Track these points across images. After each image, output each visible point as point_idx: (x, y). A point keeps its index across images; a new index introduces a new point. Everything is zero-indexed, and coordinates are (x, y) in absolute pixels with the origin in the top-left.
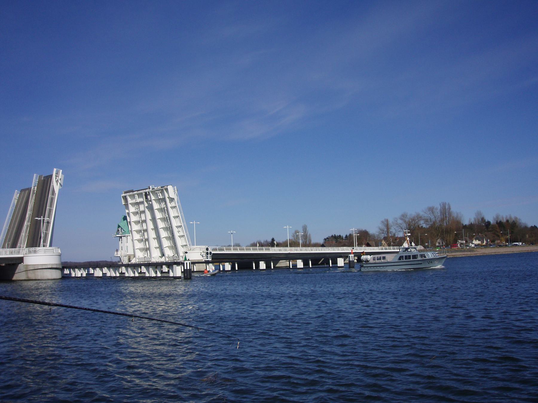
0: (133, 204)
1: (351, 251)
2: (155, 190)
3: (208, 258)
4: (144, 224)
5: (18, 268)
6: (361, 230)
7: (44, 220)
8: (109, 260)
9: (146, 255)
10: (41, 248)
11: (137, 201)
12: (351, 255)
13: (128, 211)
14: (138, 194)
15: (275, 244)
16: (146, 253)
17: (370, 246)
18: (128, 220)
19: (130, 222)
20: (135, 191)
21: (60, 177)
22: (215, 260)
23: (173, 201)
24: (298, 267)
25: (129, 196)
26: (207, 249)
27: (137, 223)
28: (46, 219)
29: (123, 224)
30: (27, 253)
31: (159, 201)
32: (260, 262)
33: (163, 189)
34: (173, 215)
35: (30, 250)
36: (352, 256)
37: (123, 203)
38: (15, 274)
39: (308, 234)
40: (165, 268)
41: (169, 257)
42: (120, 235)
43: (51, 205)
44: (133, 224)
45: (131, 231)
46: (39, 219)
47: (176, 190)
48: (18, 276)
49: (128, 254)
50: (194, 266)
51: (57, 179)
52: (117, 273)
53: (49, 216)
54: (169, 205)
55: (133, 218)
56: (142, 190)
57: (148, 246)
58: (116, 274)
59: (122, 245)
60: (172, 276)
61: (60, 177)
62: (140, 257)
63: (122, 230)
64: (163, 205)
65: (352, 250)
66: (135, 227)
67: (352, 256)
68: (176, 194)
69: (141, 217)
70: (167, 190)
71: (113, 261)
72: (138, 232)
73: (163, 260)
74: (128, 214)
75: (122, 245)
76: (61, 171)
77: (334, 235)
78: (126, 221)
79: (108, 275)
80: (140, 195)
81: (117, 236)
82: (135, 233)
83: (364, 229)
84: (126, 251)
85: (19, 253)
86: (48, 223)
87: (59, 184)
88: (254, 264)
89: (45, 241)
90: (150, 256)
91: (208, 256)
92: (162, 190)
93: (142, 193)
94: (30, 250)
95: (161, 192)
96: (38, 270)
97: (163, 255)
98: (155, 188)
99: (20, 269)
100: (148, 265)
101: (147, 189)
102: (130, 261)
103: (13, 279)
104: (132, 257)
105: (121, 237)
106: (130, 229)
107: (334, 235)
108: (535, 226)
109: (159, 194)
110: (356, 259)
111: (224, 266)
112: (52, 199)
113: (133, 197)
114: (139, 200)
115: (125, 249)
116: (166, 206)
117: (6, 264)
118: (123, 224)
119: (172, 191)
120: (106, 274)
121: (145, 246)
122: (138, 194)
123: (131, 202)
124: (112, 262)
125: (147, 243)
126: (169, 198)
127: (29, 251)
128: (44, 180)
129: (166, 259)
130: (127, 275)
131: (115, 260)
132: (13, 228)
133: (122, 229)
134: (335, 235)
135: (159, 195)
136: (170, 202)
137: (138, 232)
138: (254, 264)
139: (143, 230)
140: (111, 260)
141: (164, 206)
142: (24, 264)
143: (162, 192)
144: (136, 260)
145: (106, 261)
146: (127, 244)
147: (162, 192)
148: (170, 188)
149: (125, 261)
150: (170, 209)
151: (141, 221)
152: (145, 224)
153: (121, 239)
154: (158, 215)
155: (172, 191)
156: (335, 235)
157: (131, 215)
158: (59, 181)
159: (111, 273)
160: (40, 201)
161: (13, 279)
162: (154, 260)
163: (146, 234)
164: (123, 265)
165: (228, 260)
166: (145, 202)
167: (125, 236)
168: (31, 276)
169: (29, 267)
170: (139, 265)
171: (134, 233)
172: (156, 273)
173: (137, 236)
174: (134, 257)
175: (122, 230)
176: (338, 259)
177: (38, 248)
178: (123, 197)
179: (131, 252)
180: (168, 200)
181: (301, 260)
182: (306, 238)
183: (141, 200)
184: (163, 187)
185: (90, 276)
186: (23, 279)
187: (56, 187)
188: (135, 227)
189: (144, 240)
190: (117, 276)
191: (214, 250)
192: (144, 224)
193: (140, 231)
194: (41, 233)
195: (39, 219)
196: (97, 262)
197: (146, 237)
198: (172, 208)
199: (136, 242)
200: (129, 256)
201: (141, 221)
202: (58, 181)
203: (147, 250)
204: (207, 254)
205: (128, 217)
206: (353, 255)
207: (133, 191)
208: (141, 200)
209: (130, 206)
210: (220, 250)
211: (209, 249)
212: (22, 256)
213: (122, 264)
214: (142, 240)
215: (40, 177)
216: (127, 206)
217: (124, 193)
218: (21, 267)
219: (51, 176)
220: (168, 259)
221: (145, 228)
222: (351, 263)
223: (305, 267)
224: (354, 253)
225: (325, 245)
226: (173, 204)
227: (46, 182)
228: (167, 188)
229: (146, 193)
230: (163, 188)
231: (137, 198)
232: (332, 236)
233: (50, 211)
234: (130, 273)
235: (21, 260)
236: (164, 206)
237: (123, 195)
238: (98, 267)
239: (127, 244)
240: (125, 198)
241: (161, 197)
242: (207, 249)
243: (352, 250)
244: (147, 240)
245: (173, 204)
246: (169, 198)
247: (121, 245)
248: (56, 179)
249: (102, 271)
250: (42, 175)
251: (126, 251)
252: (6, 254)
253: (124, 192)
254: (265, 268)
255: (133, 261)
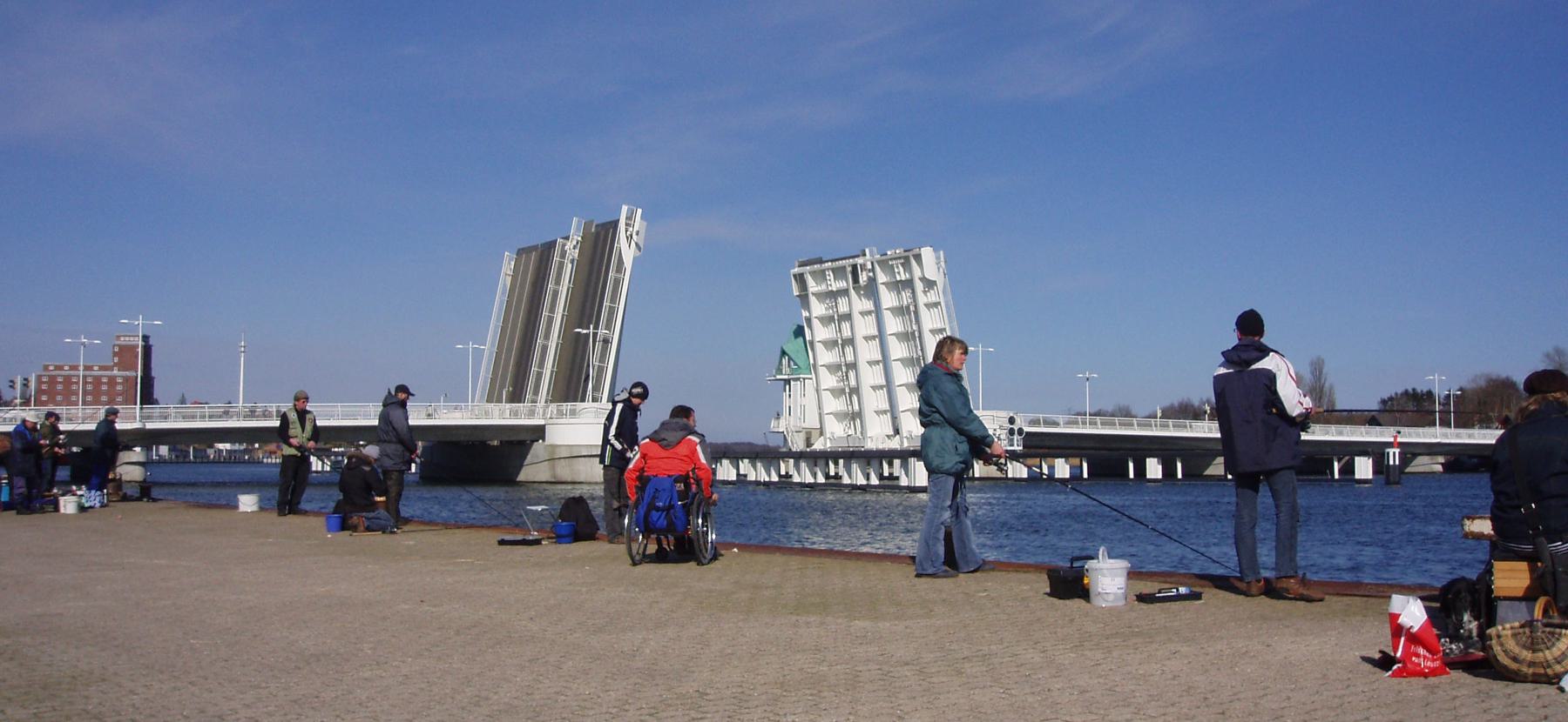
0: (821, 296)
1: (1392, 440)
2: (888, 257)
3: (1012, 445)
4: (849, 350)
5: (532, 452)
6: (1494, 377)
7: (595, 335)
8: (759, 440)
9: (851, 432)
10: (588, 404)
11: (830, 289)
12: (1391, 451)
13: (808, 314)
14: (833, 270)
15: (1206, 412)
16: (852, 425)
17: (1380, 425)
18: (808, 338)
19: (812, 343)
20: (827, 261)
21: (636, 229)
22: (1033, 451)
23: (933, 289)
24: (1357, 477)
25: (813, 273)
26: (1012, 421)
27: (830, 344)
28: (602, 332)
29: (794, 346)
30: (553, 416)
31: (897, 286)
32: (1148, 460)
33: (908, 257)
34: (931, 327)
35: (560, 408)
36: (1394, 453)
37: (796, 293)
38: (524, 468)
39: (1327, 385)
40: (728, 469)
41: (910, 438)
42: (786, 377)
43: (614, 299)
44: (819, 347)
45: (815, 366)
46: (585, 331)
47: (942, 259)
48: (533, 470)
49: (804, 425)
50: (740, 462)
51: (628, 233)
52: (773, 473)
53: (608, 326)
54: (922, 299)
55: (821, 333)
56: (842, 259)
57: (856, 408)
58: (815, 478)
59: (790, 402)
60: (906, 484)
61: (636, 229)
62: (836, 434)
63: (792, 363)
64: (906, 297)
65: (1395, 437)
66: (825, 357)
67: (1394, 453)
68: (941, 270)
69: (840, 331)
70: (918, 257)
71: (771, 445)
72: (833, 368)
73: (894, 444)
74: (809, 320)
75: (790, 402)
76: (640, 211)
77: (1410, 390)
78: (801, 339)
79: (752, 477)
80: (839, 273)
81: (778, 377)
82: (823, 372)
83: (1504, 375)
84: (800, 419)
85: (532, 414)
86: (606, 341)
87: (633, 244)
88: (1131, 465)
89: (596, 388)
90: (862, 433)
91: (1013, 440)
92: (907, 259)
93: (845, 267)
94: (560, 408)
95: (902, 264)
96: (580, 459)
97: (897, 432)
98: (889, 253)
99: (537, 457)
100: (851, 456)
101: (858, 256)
102: (809, 444)
103: (518, 479)
104: (815, 434)
105: (788, 382)
106: (812, 362)
107: (1410, 390)
108: (1223, 353)
109: (898, 267)
110: (1442, 464)
111: (1051, 468)
112: (617, 283)
113: (820, 276)
114: (836, 285)
115: (797, 411)
116: (915, 301)
117: (501, 442)
118: (794, 346)
119: (931, 263)
120: (745, 476)
121: (850, 408)
122: (833, 270)
123: (816, 289)
124: (768, 446)
125: (855, 398)
126: (923, 279)
127: (558, 410)
128: (597, 234)
129: (902, 442)
130: (796, 479)
131: (773, 442)
132: (509, 350)
133: (790, 359)
134: (1414, 390)
135: (899, 273)
136: (925, 292)
137: (833, 368)
138: (1131, 465)
139: (846, 365)
140: (764, 443)
141: (909, 301)
142: (546, 443)
143: (906, 265)
144: (826, 443)
145: (750, 444)
146: (805, 401)
147: (906, 265)
148: (927, 253)
149: (798, 445)
150: (923, 311)
151: (840, 342)
152: (851, 349)
153: (787, 387)
154: (893, 325)
155: (931, 263)
156: (1414, 390)
157: (816, 323)
158: (634, 236)
159: (756, 472)
160: (588, 285)
161: (518, 479)
162: (871, 445)
163: (852, 374)
164: (790, 454)
165: (1077, 451)
166: (852, 291)
167: (798, 379)
168: (564, 472)
169: (558, 450)
170: (834, 456)
171: (823, 372)
172: (815, 476)
173: (829, 381)
174: (821, 434)
175: (792, 363)
176: (1356, 458)
177: (580, 405)
178: (795, 276)
179: (812, 422)
180: (919, 286)
181: (1156, 459)
182: (1320, 398)
183: (842, 284)
184: (909, 251)
185: (834, 483)
186: (544, 479)
187: (627, 252)
188: (825, 357)
189: (847, 390)
190: (773, 480)
191: (1035, 422)
192: (849, 350)
193: (838, 367)
194: (588, 366)
195: (585, 331)
196: (726, 446)
197: (853, 383)
198: (928, 306)
199: (826, 396)
200: (807, 433)
201: (840, 342)
202: (631, 237)
203: (855, 416)
204: (1011, 432)
205: (807, 330)
206: (1397, 451)
207: (821, 261)
208: (842, 284)
209: (813, 300)
210: (1047, 423)
211: (1018, 421)
212: (542, 422)
213: (788, 450)
214: (842, 391)
215: (588, 225)
216: (804, 299)
217: (799, 266)
218: (538, 447)
219: (615, 224)
220: (909, 442)
221: (850, 358)
222: (1391, 470)
223: (882, 483)
224: (1401, 445)
225: (1381, 418)
226: (932, 297)
227: (602, 237)
228: (920, 255)
229: (854, 267)
230: (910, 254)
231: (832, 280)
232: (1406, 392)
233: (612, 311)
234: (804, 475)
235: (539, 432)
236: (909, 301)
237: (796, 270)
238: (727, 458)
239: (805, 401)
240: (800, 279)
241: (902, 275)
242: (1012, 421)
243: (1395, 437)
244: (856, 391)
245: (932, 297)
246: (923, 279)
247: (786, 402)
248: (626, 231)
249: (738, 469)
250: (592, 222)
251: (800, 419)
252: (502, 416)
253: (797, 264)
254: (1160, 477)
255: (818, 445)
